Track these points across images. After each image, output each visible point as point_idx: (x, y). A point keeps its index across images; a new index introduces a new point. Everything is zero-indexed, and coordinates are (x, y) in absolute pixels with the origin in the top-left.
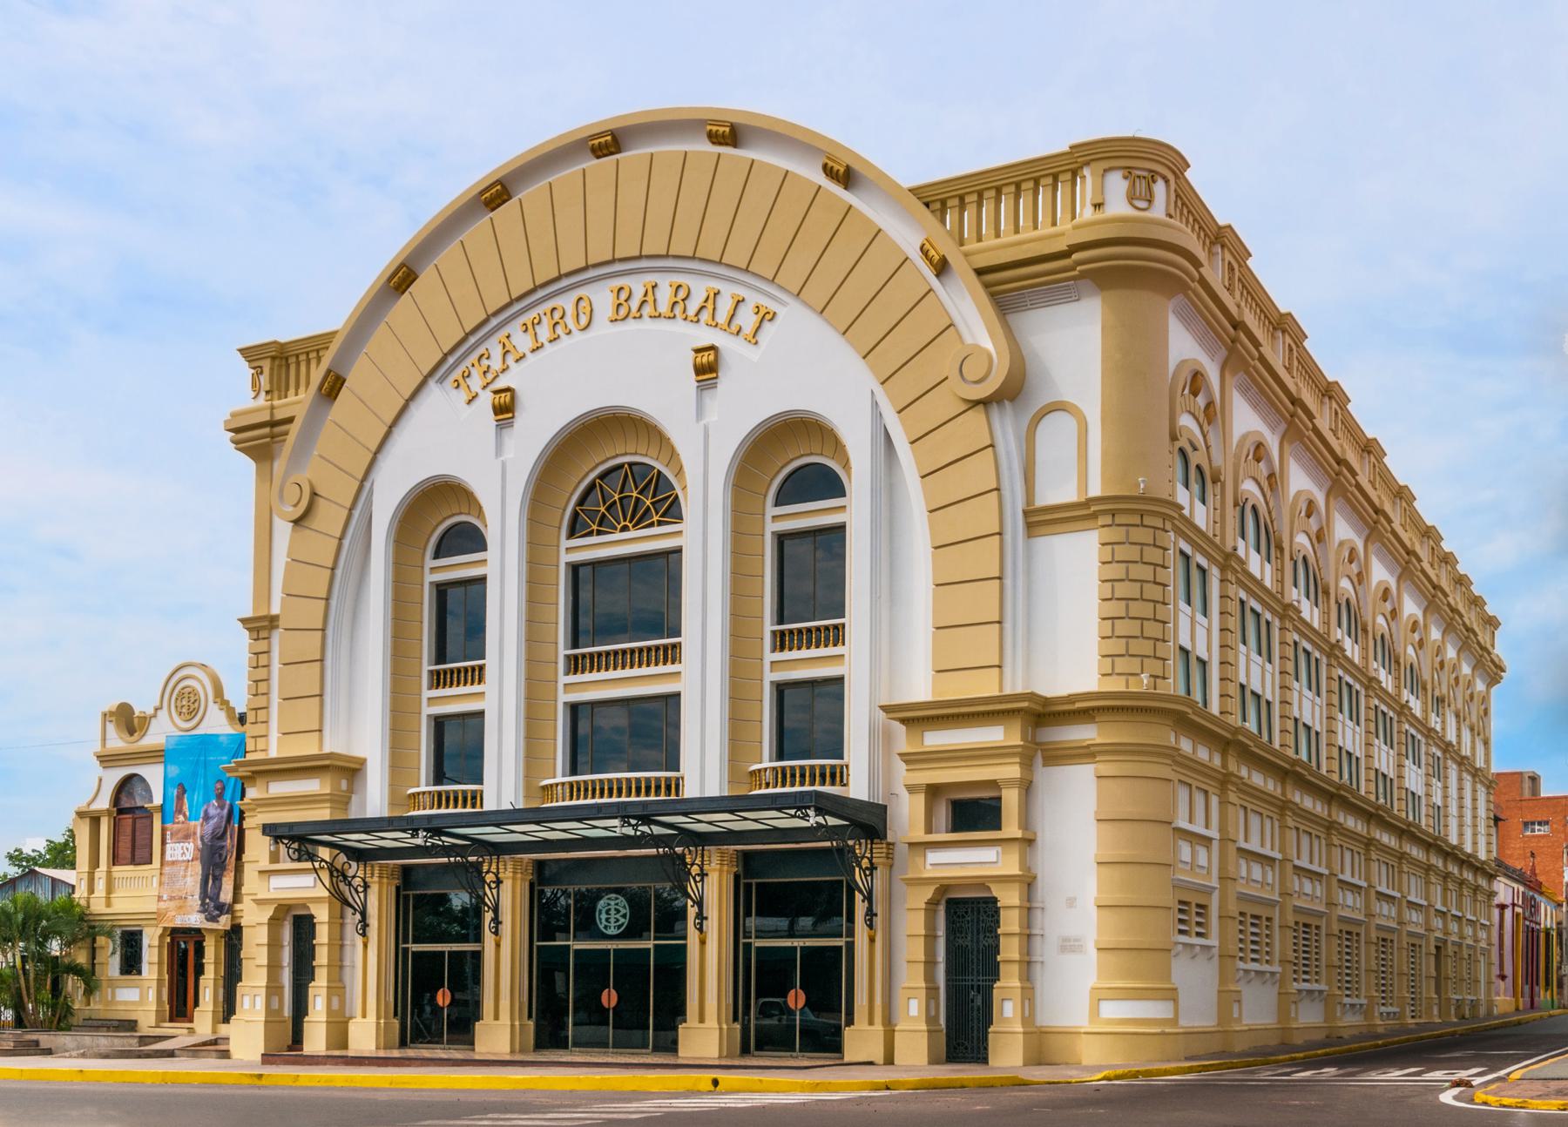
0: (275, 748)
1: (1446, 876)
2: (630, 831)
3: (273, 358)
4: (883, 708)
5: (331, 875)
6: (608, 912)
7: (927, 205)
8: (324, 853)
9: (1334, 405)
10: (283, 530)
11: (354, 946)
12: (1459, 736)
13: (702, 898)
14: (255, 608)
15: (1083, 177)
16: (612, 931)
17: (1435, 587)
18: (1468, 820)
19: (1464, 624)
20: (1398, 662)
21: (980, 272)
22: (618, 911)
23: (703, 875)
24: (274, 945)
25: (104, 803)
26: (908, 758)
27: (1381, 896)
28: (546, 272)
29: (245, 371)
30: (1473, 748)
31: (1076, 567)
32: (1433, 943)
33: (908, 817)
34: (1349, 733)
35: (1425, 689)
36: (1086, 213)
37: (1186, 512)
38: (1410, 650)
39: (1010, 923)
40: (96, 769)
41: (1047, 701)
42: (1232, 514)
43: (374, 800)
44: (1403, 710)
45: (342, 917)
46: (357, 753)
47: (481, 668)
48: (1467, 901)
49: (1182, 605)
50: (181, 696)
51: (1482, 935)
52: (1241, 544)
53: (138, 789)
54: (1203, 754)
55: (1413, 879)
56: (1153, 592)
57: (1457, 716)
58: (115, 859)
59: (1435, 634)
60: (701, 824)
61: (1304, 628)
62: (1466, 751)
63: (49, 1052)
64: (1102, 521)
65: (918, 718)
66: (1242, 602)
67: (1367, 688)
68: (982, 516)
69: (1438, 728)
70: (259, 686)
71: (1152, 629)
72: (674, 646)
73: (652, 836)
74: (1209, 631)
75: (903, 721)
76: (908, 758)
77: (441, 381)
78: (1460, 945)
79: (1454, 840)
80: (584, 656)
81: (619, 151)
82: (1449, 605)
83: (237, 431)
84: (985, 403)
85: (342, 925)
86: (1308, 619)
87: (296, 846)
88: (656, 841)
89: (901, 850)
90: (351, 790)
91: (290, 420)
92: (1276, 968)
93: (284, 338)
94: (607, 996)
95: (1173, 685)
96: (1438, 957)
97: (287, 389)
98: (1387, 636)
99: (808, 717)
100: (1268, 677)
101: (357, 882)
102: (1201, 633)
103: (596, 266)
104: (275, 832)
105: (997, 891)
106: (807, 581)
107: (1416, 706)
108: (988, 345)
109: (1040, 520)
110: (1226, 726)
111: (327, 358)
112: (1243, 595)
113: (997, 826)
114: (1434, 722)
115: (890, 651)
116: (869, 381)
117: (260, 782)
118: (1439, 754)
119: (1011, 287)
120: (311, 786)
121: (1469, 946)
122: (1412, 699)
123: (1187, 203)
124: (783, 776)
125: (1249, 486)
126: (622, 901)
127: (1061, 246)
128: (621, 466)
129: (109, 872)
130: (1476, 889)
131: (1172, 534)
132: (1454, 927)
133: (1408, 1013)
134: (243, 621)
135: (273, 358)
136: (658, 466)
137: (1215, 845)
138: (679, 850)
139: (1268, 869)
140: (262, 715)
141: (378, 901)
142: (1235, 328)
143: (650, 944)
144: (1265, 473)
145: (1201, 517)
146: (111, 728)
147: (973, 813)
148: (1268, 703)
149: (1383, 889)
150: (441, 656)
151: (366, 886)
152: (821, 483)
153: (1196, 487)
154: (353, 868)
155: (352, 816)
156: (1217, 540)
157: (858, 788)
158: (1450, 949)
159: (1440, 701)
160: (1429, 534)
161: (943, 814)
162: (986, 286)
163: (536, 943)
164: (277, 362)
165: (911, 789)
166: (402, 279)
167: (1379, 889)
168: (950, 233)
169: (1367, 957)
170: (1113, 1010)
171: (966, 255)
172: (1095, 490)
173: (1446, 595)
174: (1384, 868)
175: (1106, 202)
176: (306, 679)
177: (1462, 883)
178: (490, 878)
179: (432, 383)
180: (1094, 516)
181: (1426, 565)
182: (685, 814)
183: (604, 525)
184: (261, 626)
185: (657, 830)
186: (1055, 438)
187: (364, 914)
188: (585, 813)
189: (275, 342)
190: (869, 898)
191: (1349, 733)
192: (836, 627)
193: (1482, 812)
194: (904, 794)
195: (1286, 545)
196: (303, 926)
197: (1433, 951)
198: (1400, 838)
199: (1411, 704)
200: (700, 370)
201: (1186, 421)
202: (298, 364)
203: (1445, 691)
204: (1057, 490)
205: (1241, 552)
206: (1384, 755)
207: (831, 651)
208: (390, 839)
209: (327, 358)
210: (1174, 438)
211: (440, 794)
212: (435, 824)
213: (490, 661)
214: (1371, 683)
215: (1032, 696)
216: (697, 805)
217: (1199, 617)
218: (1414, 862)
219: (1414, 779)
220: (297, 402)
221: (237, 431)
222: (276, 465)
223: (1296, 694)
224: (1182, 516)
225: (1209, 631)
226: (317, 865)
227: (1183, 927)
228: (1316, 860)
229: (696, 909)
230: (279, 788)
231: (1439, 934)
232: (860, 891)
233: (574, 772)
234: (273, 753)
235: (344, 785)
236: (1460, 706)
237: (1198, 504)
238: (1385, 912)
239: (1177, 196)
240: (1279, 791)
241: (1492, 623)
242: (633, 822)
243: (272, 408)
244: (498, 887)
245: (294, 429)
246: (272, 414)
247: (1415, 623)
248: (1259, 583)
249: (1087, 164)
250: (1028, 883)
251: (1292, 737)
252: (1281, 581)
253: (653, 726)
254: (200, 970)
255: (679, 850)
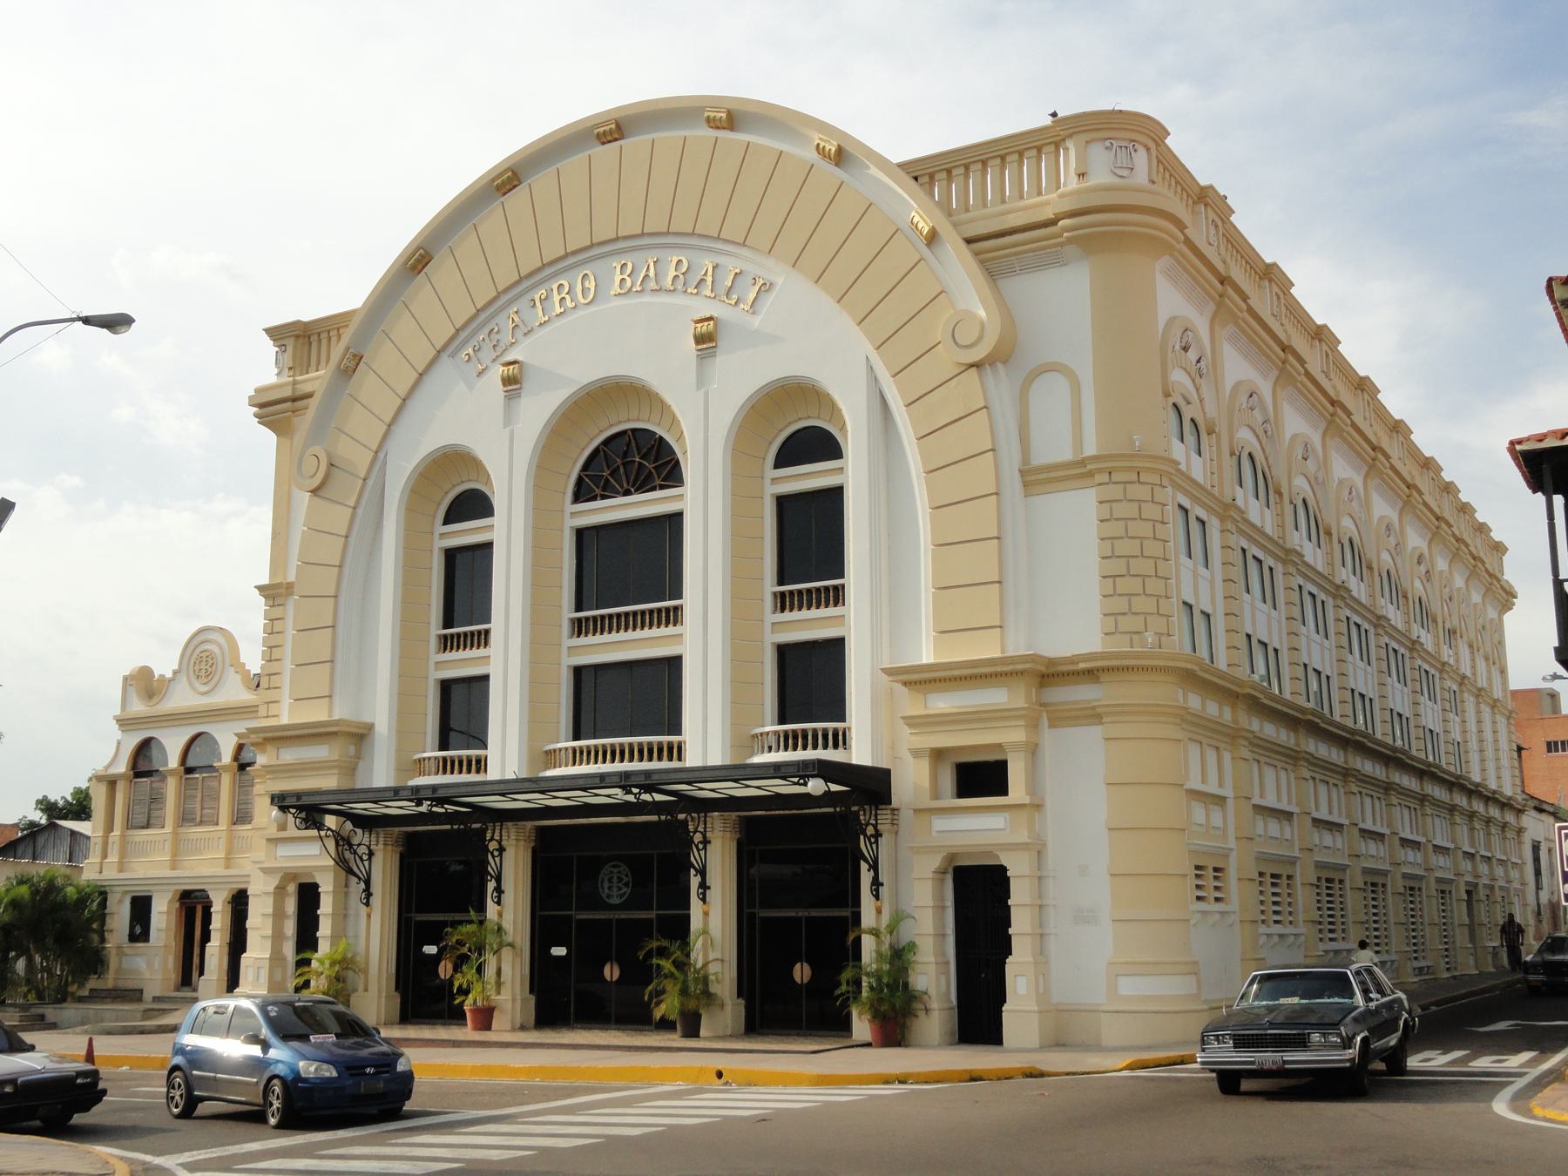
0: (286, 715)
1: (1472, 815)
2: (631, 798)
3: (297, 337)
4: (884, 670)
5: (337, 844)
6: (610, 881)
7: (916, 179)
8: (331, 821)
9: (1325, 348)
10: (303, 499)
11: (358, 915)
12: (1473, 667)
13: (705, 866)
14: (273, 572)
15: (1066, 149)
16: (615, 901)
17: (1333, 403)
18: (1490, 753)
19: (1471, 554)
20: (1405, 597)
21: (969, 241)
22: (620, 880)
23: (706, 842)
24: (278, 915)
25: (122, 767)
26: (911, 722)
27: (1405, 842)
28: (577, 239)
29: (269, 348)
30: (1489, 679)
31: (1075, 518)
32: (1463, 889)
33: (913, 781)
34: (1360, 674)
35: (1435, 621)
36: (1070, 183)
37: (1183, 467)
38: (1418, 584)
39: (1019, 896)
40: (115, 732)
41: (1052, 662)
42: (1229, 464)
43: (381, 772)
44: (1414, 645)
45: (347, 886)
46: (367, 719)
47: (487, 632)
48: (1495, 840)
49: (1184, 559)
50: (200, 660)
51: (1514, 874)
52: (1239, 492)
53: (155, 752)
54: (1212, 709)
55: (1437, 821)
56: (1153, 548)
57: (1471, 646)
58: (130, 825)
59: (1442, 564)
60: (707, 791)
61: (1308, 572)
62: (1482, 682)
63: (53, 1026)
64: (1099, 478)
65: (922, 680)
66: (1244, 550)
67: (1376, 626)
68: (980, 476)
69: (1452, 661)
70: (272, 651)
71: (1154, 586)
72: (676, 608)
73: (655, 803)
74: (1212, 582)
75: (905, 684)
76: (911, 722)
77: (453, 355)
78: (1492, 888)
79: (1476, 778)
80: (587, 619)
81: (622, 138)
82: (1454, 535)
83: (261, 406)
84: (976, 365)
85: (346, 894)
86: (1311, 562)
87: (303, 815)
88: (656, 807)
89: (906, 816)
90: (358, 756)
91: (310, 396)
92: (1302, 929)
93: (306, 317)
94: (601, 973)
95: (1179, 643)
96: (1469, 902)
97: (319, 363)
98: (1393, 572)
99: (809, 681)
100: (1274, 623)
101: (363, 850)
102: (1204, 586)
103: (626, 238)
104: (282, 802)
105: (1005, 860)
106: (809, 541)
107: (1427, 639)
108: (982, 313)
109: (1037, 479)
110: (1235, 681)
111: (347, 335)
112: (1244, 543)
113: (1003, 791)
114: (1446, 654)
115: (885, 622)
116: (862, 346)
117: (270, 749)
118: (1455, 687)
119: (999, 250)
120: (320, 752)
121: (1501, 888)
122: (1423, 633)
123: (1169, 168)
124: (790, 741)
125: (1244, 435)
126: (623, 867)
127: (1048, 214)
128: (624, 433)
129: (123, 836)
130: (1504, 826)
131: (1169, 489)
132: (1483, 868)
133: (1443, 965)
134: (261, 588)
135: (297, 337)
136: (660, 432)
137: (1230, 803)
138: (681, 816)
139: (1285, 823)
140: (275, 681)
141: (384, 869)
142: (1222, 283)
143: (652, 915)
144: (1260, 420)
145: (1197, 469)
146: (132, 692)
147: (981, 778)
148: (1276, 650)
149: (1407, 835)
150: (448, 622)
151: (371, 854)
152: (814, 445)
153: (1190, 438)
154: (360, 836)
155: (359, 786)
156: (1216, 491)
157: (860, 753)
158: (1482, 893)
159: (1451, 633)
160: (1428, 465)
161: (948, 780)
162: (976, 254)
163: (539, 913)
164: (299, 339)
165: (916, 753)
166: (418, 261)
167: (1403, 835)
168: (939, 204)
169: (1395, 908)
170: (1127, 986)
171: (955, 225)
172: (1090, 449)
173: (1450, 526)
174: (1406, 812)
175: (1067, 180)
176: (320, 644)
177: (1488, 821)
178: (493, 846)
179: (444, 356)
180: (1091, 474)
181: (1427, 498)
182: (689, 783)
183: (607, 491)
184: (273, 593)
185: (659, 797)
186: (1051, 400)
187: (368, 883)
188: (589, 782)
189: (298, 322)
190: (874, 867)
191: (1360, 674)
192: (836, 588)
193: (1504, 744)
194: (908, 757)
195: (1285, 491)
196: (308, 896)
197: (1465, 897)
198: (1421, 779)
199: (1422, 640)
200: (700, 339)
201: (1178, 376)
202: (320, 341)
203: (1455, 622)
204: (1054, 447)
205: (1240, 502)
206: (1398, 693)
207: (832, 611)
208: (394, 808)
209: (347, 335)
210: (1167, 395)
211: (445, 759)
212: (441, 793)
213: (496, 626)
214: (1380, 621)
215: (1034, 658)
216: (697, 774)
217: (1202, 570)
218: (1437, 804)
219: (1431, 716)
220: (317, 379)
221: (261, 406)
222: (296, 439)
223: (1303, 639)
224: (1179, 471)
225: (1212, 582)
226: (323, 833)
227: (1200, 893)
228: (1336, 811)
229: (699, 878)
230: (289, 755)
231: (1469, 878)
232: (866, 861)
233: (576, 737)
234: (285, 720)
235: (352, 750)
236: (1472, 636)
237: (1194, 456)
238: (1411, 859)
239: (1159, 161)
240: (1292, 741)
241: (1499, 548)
242: (635, 790)
243: (295, 383)
244: (501, 855)
245: (313, 403)
246: (294, 390)
247: (1420, 556)
248: (1260, 531)
249: (1070, 136)
250: (1039, 851)
251: (1303, 684)
252: (1282, 526)
253: (651, 694)
254: (206, 937)
255: (681, 816)
